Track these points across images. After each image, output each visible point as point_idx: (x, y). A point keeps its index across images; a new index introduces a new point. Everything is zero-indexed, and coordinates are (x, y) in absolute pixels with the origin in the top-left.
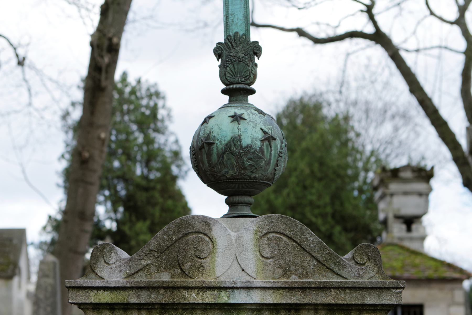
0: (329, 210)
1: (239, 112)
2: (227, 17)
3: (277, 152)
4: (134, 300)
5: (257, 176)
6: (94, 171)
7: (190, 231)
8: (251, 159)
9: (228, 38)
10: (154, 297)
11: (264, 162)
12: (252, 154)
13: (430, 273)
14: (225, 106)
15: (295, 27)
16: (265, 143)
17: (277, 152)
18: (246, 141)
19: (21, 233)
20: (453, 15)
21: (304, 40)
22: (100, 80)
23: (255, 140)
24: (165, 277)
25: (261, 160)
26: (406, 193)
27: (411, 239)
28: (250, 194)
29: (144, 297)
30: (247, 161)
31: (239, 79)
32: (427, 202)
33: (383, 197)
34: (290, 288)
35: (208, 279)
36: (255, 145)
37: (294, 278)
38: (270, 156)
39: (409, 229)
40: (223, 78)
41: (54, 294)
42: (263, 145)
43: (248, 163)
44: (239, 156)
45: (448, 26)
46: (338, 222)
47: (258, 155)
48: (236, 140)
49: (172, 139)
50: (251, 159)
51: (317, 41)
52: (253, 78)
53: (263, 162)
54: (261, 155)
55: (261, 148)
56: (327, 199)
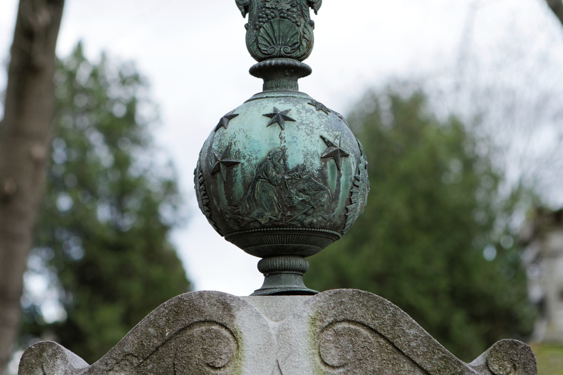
0: (443, 283)
1: (281, 107)
3: (351, 178)
5: (315, 220)
7: (195, 320)
8: (303, 191)
11: (326, 196)
12: (306, 182)
14: (256, 98)
16: (328, 163)
17: (351, 178)
23: (311, 158)
25: (322, 192)
30: (297, 195)
31: (282, 50)
36: (311, 166)
38: (337, 185)
42: (325, 166)
43: (299, 197)
44: (283, 186)
47: (316, 183)
50: (303, 191)
52: (306, 48)
53: (325, 197)
54: (321, 184)
55: (321, 171)
56: (439, 264)
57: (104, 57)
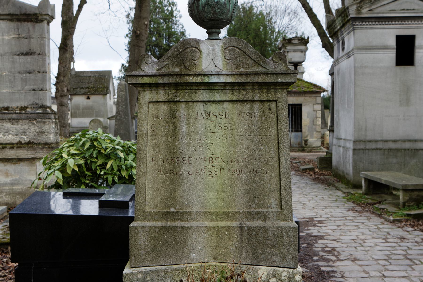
4: (161, 81)
6: (143, 41)
10: (171, 80)
13: (305, 89)
24: (177, 70)
26: (295, 51)
29: (166, 80)
32: (305, 55)
34: (240, 74)
44: (213, 7)
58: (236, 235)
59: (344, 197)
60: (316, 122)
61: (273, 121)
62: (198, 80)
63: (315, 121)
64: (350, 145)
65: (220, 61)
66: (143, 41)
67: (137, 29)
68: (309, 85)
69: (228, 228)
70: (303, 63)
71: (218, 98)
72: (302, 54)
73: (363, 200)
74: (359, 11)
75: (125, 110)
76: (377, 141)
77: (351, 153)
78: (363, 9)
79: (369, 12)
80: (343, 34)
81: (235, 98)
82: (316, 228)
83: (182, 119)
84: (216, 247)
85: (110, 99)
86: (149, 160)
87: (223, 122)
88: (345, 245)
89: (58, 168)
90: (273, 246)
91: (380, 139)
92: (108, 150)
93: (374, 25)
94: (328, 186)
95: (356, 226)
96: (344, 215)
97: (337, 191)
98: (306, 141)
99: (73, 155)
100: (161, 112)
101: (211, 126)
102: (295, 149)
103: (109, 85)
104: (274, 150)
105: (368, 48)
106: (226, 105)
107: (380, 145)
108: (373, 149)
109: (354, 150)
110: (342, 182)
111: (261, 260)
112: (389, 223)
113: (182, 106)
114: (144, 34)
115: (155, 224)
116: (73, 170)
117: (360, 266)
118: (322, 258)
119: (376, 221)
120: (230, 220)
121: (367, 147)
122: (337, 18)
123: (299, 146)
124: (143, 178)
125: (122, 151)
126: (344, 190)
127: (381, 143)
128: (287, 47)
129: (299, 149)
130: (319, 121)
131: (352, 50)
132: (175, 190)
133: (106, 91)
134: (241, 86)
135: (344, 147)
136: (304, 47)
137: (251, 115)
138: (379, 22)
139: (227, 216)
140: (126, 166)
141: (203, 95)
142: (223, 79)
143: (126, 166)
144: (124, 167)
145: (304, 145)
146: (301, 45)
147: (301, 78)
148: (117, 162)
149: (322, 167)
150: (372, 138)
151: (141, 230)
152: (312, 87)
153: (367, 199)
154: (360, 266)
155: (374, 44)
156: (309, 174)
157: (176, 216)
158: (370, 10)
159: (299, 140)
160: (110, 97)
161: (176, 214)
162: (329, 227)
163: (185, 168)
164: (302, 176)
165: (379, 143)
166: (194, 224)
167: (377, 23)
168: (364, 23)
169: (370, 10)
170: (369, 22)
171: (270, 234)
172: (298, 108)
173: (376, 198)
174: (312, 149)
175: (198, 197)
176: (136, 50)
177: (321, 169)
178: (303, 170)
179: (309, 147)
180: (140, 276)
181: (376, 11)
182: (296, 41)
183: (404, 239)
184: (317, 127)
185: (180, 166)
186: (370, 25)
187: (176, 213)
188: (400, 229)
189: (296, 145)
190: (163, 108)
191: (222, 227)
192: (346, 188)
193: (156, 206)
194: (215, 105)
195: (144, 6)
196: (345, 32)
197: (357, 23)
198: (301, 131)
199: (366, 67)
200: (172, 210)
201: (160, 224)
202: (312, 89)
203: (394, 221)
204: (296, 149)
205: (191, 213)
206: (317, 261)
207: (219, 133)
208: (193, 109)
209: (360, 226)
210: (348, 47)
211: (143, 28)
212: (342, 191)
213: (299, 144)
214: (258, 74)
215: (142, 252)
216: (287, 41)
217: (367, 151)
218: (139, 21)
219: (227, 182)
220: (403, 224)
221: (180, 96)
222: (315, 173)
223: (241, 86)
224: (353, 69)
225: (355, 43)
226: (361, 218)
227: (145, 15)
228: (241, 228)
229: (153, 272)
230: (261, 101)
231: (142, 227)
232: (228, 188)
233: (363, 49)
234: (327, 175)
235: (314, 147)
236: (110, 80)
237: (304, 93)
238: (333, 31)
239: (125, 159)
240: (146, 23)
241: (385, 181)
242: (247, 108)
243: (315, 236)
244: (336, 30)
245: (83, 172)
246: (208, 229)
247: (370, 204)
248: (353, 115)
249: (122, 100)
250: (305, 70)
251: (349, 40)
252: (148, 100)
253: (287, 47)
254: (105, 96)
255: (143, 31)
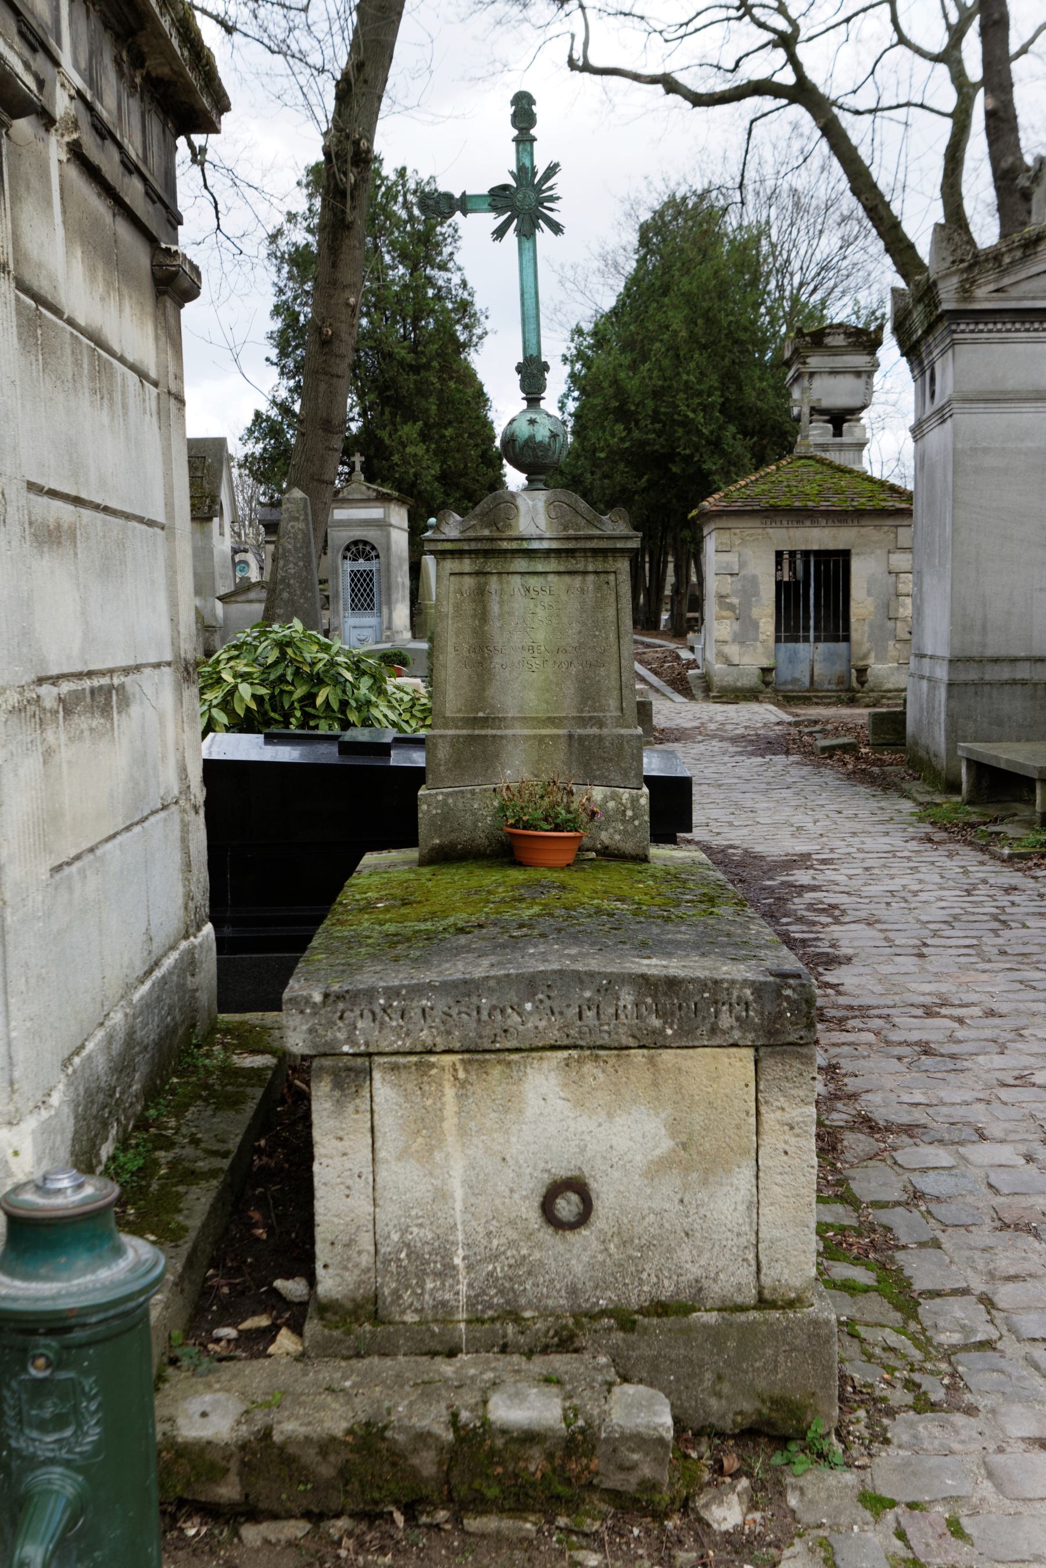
0: (716, 398)
1: (533, 416)
2: (524, 343)
4: (466, 547)
6: (342, 357)
9: (525, 358)
10: (480, 546)
13: (861, 502)
14: (524, 411)
15: (658, 71)
18: (539, 438)
19: (220, 444)
20: (937, 40)
21: (675, 98)
22: (343, 212)
24: (486, 532)
26: (834, 372)
27: (841, 447)
28: (541, 474)
29: (473, 546)
32: (869, 385)
33: (797, 379)
34: (568, 539)
35: (514, 533)
37: (571, 532)
39: (838, 432)
40: (523, 388)
41: (307, 543)
44: (534, 449)
45: (927, 64)
46: (730, 419)
48: (532, 437)
49: (456, 279)
51: (698, 100)
56: (713, 380)
57: (402, 173)
58: (563, 746)
59: (912, 814)
60: (897, 610)
61: (612, 599)
62: (514, 545)
63: (893, 604)
64: (942, 673)
65: (542, 521)
66: (342, 357)
67: (323, 320)
68: (875, 487)
69: (552, 737)
70: (864, 414)
71: (540, 568)
72: (859, 383)
73: (961, 818)
74: (965, 291)
75: (304, 574)
76: (1014, 660)
77: (942, 693)
78: (979, 286)
79: (994, 295)
80: (931, 353)
81: (562, 569)
82: (812, 871)
83: (494, 597)
84: (537, 762)
85: (222, 534)
86: (450, 649)
87: (547, 599)
88: (867, 901)
89: (215, 702)
90: (611, 760)
91: (1022, 654)
92: (321, 665)
93: (1009, 331)
94: (884, 789)
95: (911, 868)
96: (890, 848)
97: (903, 800)
98: (862, 671)
99: (245, 677)
100: (466, 587)
101: (532, 605)
102: (826, 697)
103: (218, 488)
104: (612, 636)
105: (1001, 397)
106: (551, 577)
107: (1023, 672)
108: (1005, 683)
109: (951, 685)
110: (925, 780)
111: (595, 778)
112: (998, 863)
113: (494, 579)
114: (344, 336)
115: (458, 732)
116: (248, 709)
117: (881, 930)
118: (801, 920)
119: (969, 857)
120: (557, 727)
121: (987, 677)
122: (915, 306)
123: (841, 687)
124: (443, 673)
125: (348, 669)
126: (921, 798)
127: (1027, 664)
128: (808, 360)
129: (838, 697)
130: (904, 606)
131: (949, 402)
132: (484, 689)
133: (210, 507)
134: (570, 553)
135: (929, 680)
136: (867, 358)
137: (583, 591)
138: (1023, 323)
139: (552, 721)
140: (356, 700)
141: (521, 564)
142: (545, 545)
143: (356, 700)
144: (353, 704)
145: (855, 684)
146: (856, 352)
147: (856, 467)
148: (339, 692)
149: (881, 741)
150: (1002, 653)
151: (440, 740)
152: (882, 496)
153: (968, 813)
154: (881, 930)
155: (1010, 385)
156: (839, 760)
157: (485, 722)
158: (997, 291)
159: (840, 668)
160: (221, 526)
161: (486, 719)
162: (842, 871)
163: (497, 660)
164: (819, 767)
165: (1019, 664)
166: (509, 732)
167: (1018, 326)
168: (981, 327)
169: (997, 291)
170: (995, 323)
171: (607, 744)
172: (836, 563)
173: (993, 811)
174: (883, 697)
175: (514, 698)
176: (323, 387)
177: (875, 746)
178: (824, 749)
179: (872, 691)
180: (440, 798)
181: (1014, 292)
182: (839, 340)
183: (1016, 889)
184: (899, 624)
185: (491, 658)
186: (999, 331)
187: (486, 719)
188: (1020, 874)
189: (830, 683)
190: (469, 582)
191: (545, 736)
192: (928, 793)
193: (460, 711)
194: (536, 578)
195: (344, 247)
196: (936, 346)
197: (962, 327)
198: (847, 639)
199: (986, 450)
200: (481, 714)
201: (464, 732)
202: (884, 500)
203: (1011, 857)
204: (830, 697)
205: (505, 718)
206: (787, 924)
207: (541, 613)
208: (508, 582)
209: (923, 869)
210: (943, 392)
211: (343, 318)
212: (915, 800)
213: (840, 682)
214: (591, 538)
215: (442, 768)
216: (808, 339)
217: (987, 689)
218: (331, 297)
219: (551, 677)
220: (1030, 864)
221: (491, 566)
222: (858, 759)
223: (570, 553)
224: (951, 457)
225: (955, 383)
226: (936, 853)
227: (346, 275)
228: (570, 736)
229: (456, 792)
230: (596, 573)
231: (441, 736)
232: (554, 686)
233: (979, 401)
234: (891, 764)
235: (890, 691)
236: (221, 471)
237: (857, 515)
238: (909, 339)
239: (355, 687)
240: (352, 300)
241: (1007, 760)
242: (578, 580)
243: (801, 886)
244: (915, 337)
245: (266, 713)
246: (527, 738)
247: (972, 826)
248: (948, 588)
249: (295, 547)
250: (868, 435)
251: (944, 370)
252: (449, 571)
253: (808, 360)
254: (206, 525)
255: (344, 328)
